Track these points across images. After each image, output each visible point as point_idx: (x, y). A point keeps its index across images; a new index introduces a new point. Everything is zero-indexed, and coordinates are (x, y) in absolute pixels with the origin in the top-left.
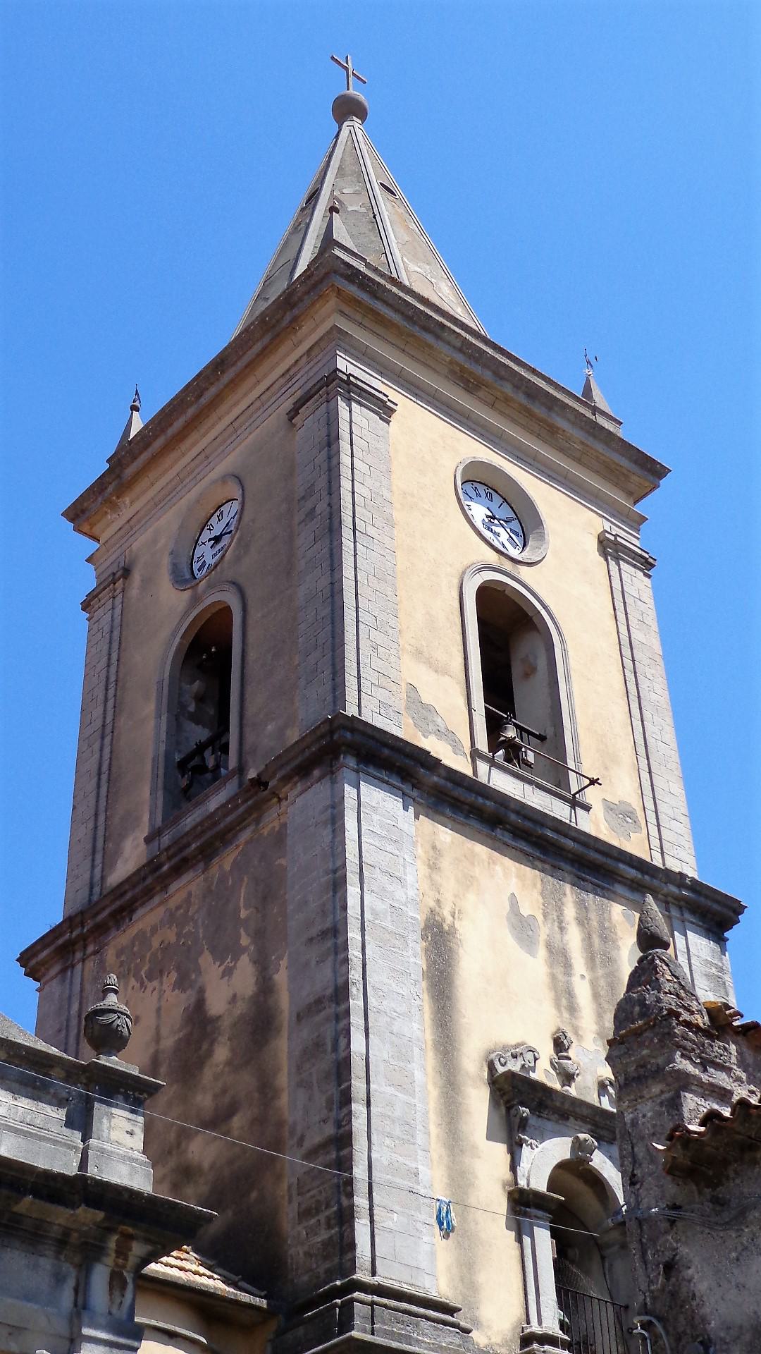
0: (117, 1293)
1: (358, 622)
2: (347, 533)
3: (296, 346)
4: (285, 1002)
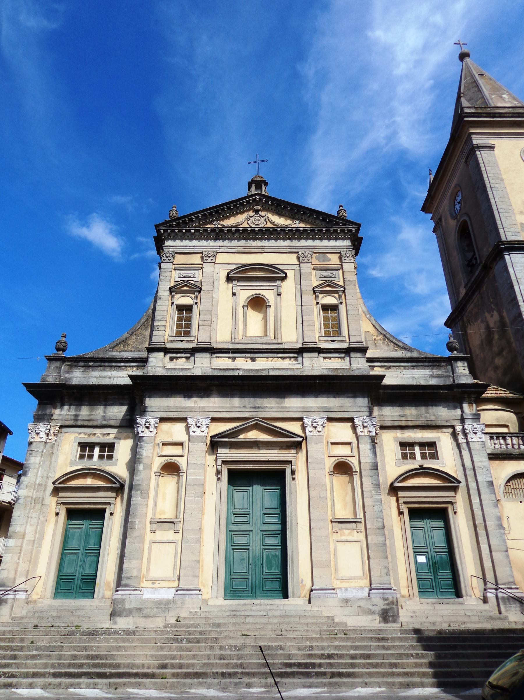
0: (471, 407)
1: (499, 213)
2: (489, 190)
3: (462, 142)
4: (507, 320)
